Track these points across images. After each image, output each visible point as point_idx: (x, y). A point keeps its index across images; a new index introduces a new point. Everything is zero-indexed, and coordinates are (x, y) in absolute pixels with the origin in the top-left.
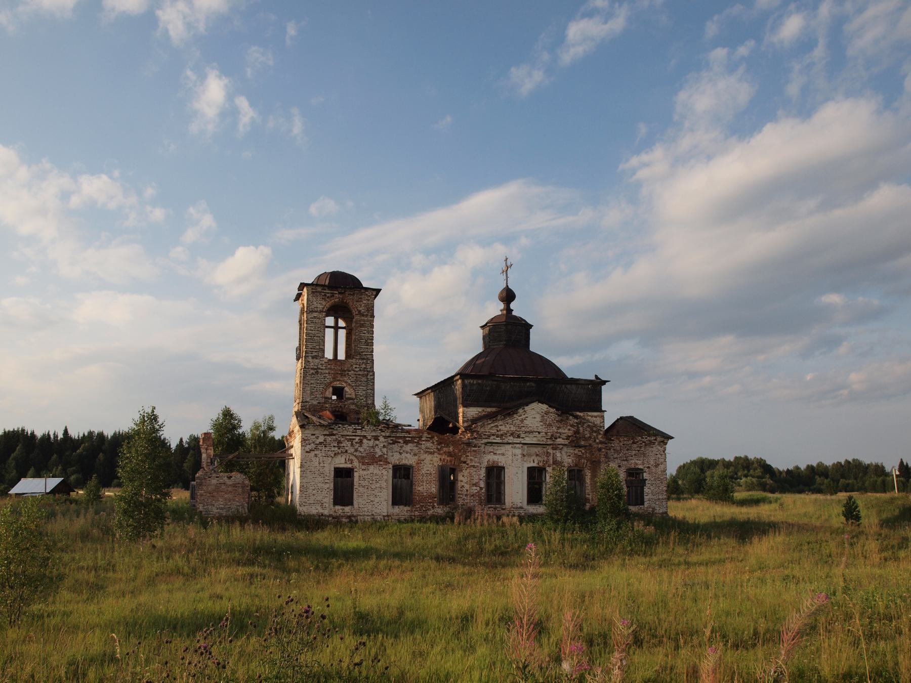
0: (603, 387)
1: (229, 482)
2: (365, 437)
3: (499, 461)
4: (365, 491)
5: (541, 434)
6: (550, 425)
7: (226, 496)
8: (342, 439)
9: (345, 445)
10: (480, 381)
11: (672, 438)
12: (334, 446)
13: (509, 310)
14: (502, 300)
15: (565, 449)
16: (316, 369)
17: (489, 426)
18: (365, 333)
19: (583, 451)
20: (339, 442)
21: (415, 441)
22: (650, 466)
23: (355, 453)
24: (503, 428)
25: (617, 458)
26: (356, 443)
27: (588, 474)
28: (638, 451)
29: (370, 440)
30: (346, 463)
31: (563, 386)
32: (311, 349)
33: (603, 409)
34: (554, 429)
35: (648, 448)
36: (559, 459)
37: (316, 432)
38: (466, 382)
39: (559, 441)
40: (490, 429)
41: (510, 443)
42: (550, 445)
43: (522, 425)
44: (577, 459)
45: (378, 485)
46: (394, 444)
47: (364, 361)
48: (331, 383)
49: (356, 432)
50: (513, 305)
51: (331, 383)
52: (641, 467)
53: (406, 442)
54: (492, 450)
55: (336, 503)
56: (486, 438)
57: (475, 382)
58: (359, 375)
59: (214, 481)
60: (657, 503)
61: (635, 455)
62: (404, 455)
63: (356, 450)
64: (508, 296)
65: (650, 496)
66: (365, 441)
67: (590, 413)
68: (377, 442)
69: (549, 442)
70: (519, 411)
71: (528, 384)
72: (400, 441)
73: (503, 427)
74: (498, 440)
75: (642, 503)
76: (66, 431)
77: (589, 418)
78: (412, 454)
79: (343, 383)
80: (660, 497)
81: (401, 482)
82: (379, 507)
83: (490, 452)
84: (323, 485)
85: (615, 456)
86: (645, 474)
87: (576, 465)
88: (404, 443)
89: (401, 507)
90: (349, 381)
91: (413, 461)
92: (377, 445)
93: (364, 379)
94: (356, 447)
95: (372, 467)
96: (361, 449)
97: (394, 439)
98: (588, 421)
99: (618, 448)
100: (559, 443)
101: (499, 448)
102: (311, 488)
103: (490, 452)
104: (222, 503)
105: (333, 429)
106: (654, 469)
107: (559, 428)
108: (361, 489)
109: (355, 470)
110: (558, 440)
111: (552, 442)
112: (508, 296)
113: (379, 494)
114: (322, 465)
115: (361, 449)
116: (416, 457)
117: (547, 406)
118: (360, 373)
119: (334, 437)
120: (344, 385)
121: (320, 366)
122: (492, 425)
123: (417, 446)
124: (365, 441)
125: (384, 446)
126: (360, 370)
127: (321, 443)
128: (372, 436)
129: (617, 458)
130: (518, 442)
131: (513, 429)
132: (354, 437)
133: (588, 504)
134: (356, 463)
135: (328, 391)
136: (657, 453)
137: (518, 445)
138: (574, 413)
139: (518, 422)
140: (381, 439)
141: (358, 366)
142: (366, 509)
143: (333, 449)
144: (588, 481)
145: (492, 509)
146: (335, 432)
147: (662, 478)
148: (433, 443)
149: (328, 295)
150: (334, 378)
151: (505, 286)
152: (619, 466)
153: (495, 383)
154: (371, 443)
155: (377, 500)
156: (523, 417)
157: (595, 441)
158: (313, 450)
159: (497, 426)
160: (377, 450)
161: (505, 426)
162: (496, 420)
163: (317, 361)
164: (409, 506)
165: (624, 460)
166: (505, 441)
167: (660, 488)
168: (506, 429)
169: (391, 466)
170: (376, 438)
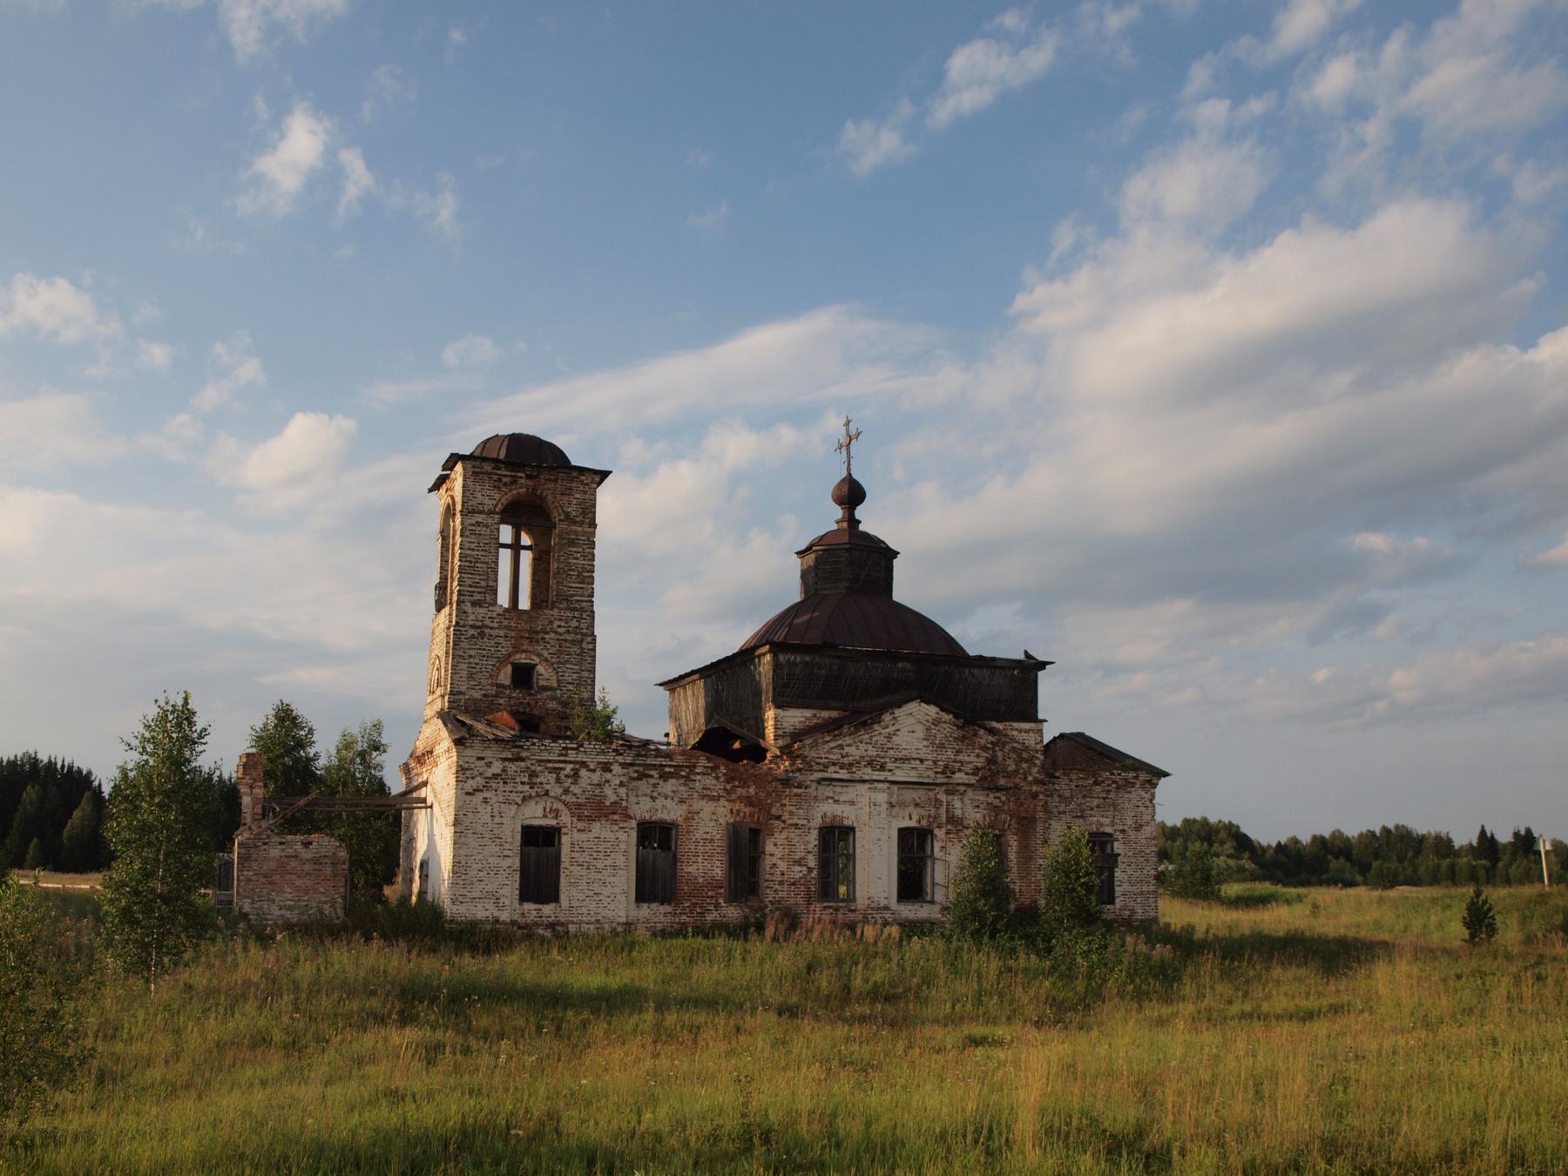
0: (1041, 674)
1: (306, 854)
2: (584, 764)
4: (584, 872)
5: (926, 763)
6: (942, 746)
9: (543, 780)
10: (808, 658)
11: (1166, 775)
12: (523, 783)
14: (839, 500)
20: (533, 774)
21: (683, 773)
22: (1125, 828)
23: (563, 797)
25: (1064, 812)
26: (567, 776)
29: (594, 771)
30: (545, 816)
33: (1041, 716)
36: (958, 813)
38: (782, 658)
39: (960, 777)
43: (889, 745)
48: (509, 655)
49: (566, 755)
50: (860, 512)
52: (1109, 830)
53: (665, 777)
54: (831, 794)
58: (566, 640)
63: (566, 791)
64: (851, 495)
65: (1126, 887)
66: (583, 772)
67: (1016, 725)
68: (608, 776)
69: (941, 779)
71: (900, 665)
73: (853, 748)
74: (843, 774)
77: (1015, 733)
79: (534, 657)
80: (1145, 888)
83: (828, 798)
85: (1061, 809)
88: (661, 777)
89: (654, 906)
90: (545, 654)
91: (678, 813)
92: (607, 781)
94: (566, 785)
95: (596, 826)
97: (641, 769)
98: (1013, 740)
100: (960, 781)
103: (828, 798)
104: (290, 896)
107: (959, 752)
110: (958, 775)
111: (945, 780)
112: (851, 495)
113: (611, 879)
118: (568, 637)
119: (523, 764)
121: (488, 622)
122: (832, 744)
123: (685, 785)
124: (583, 772)
126: (568, 632)
127: (495, 776)
128: (599, 763)
129: (1064, 812)
130: (882, 778)
131: (872, 752)
132: (561, 765)
134: (566, 818)
136: (1140, 804)
137: (880, 785)
138: (987, 723)
139: (881, 740)
140: (616, 769)
141: (563, 624)
142: (585, 910)
145: (831, 910)
146: (524, 754)
147: (1147, 851)
148: (717, 778)
149: (504, 480)
151: (844, 474)
153: (838, 661)
154: (596, 777)
155: (606, 891)
156: (891, 729)
158: (481, 791)
159: (841, 747)
160: (608, 791)
161: (857, 747)
164: (670, 904)
165: (1077, 817)
166: (857, 776)
169: (634, 824)
170: (606, 768)
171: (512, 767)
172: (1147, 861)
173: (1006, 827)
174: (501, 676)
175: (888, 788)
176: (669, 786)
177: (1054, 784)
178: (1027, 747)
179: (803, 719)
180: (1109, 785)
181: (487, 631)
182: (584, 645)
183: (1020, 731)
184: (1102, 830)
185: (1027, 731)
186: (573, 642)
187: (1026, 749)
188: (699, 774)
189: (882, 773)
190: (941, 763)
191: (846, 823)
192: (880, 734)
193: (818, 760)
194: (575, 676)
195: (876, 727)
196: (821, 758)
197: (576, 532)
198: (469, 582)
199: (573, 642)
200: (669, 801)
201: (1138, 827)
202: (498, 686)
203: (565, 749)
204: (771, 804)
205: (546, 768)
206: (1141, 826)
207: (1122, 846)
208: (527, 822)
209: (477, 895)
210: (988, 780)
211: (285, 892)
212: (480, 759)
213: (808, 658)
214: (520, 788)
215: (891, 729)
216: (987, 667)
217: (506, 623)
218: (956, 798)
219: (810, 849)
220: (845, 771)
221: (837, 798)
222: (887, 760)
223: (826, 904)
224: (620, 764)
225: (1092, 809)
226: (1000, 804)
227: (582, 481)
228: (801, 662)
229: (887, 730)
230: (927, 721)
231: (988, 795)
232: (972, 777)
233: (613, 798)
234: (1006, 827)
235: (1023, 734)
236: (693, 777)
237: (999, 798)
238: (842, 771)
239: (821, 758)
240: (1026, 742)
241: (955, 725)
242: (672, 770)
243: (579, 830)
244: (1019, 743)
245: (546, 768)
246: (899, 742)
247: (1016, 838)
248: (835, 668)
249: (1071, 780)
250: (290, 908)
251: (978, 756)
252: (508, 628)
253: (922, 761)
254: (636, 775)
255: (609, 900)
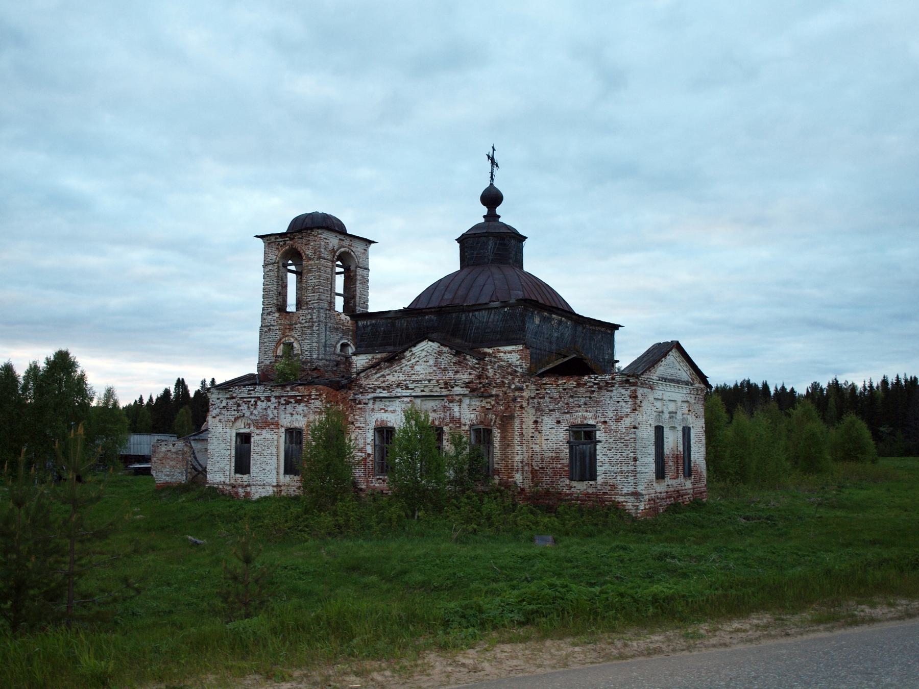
1: (173, 450)
2: (259, 398)
3: (388, 420)
4: (259, 457)
5: (432, 382)
6: (445, 370)
7: (171, 463)
8: (241, 402)
9: (243, 408)
10: (374, 322)
12: (234, 410)
13: (492, 217)
15: (466, 401)
16: (268, 326)
17: (375, 377)
18: (311, 280)
19: (493, 403)
20: (239, 405)
21: (305, 400)
22: (607, 420)
23: (251, 417)
24: (390, 378)
25: (553, 410)
26: (252, 405)
27: (497, 433)
28: (590, 398)
29: (263, 401)
30: (245, 427)
31: (471, 314)
32: (267, 305)
34: (451, 374)
35: (604, 392)
36: (457, 415)
37: (220, 396)
38: (360, 323)
39: (458, 390)
40: (376, 380)
41: (399, 397)
42: (446, 396)
43: (413, 372)
44: (483, 414)
45: (269, 452)
46: (288, 404)
47: (310, 311)
48: (280, 340)
49: (250, 394)
50: (499, 210)
51: (280, 340)
52: (591, 422)
53: (298, 402)
54: (383, 407)
55: (236, 472)
56: (373, 392)
57: (369, 324)
58: (305, 327)
59: (163, 449)
60: (619, 478)
61: (585, 404)
62: (295, 416)
63: (252, 414)
64: (492, 198)
65: (607, 467)
66: (259, 403)
67: (501, 349)
68: (269, 404)
69: (445, 392)
70: (405, 354)
71: (427, 317)
72: (292, 400)
73: (391, 376)
74: (385, 394)
75: (593, 477)
76: (792, 389)
77: (502, 354)
78: (302, 415)
79: (291, 339)
80: (625, 468)
81: (292, 447)
82: (269, 476)
83: (381, 409)
84: (225, 451)
85: (552, 407)
86: (598, 433)
87: (482, 422)
88: (296, 402)
89: (292, 476)
90: (296, 336)
91: (303, 423)
92: (269, 407)
93: (309, 331)
94: (252, 410)
95: (264, 432)
96: (255, 412)
97: (287, 398)
98: (501, 360)
99: (556, 395)
100: (458, 393)
101: (391, 403)
102: (216, 455)
103: (381, 409)
104: (168, 470)
105: (231, 391)
106: (613, 425)
107: (457, 372)
108: (255, 455)
109: (252, 435)
110: (456, 389)
111: (448, 393)
112: (492, 198)
113: (269, 461)
114: (225, 430)
115: (255, 412)
116: (306, 419)
117: (439, 345)
118: (306, 325)
119: (234, 400)
120: (292, 340)
121: (272, 323)
122: (378, 375)
123: (306, 406)
124: (259, 403)
125: (275, 408)
126: (306, 322)
127: (224, 407)
128: (266, 397)
129: (553, 410)
130: (408, 394)
131: (402, 378)
132: (249, 400)
133: (496, 477)
135: (279, 348)
136: (620, 400)
137: (406, 399)
138: (481, 349)
139: (407, 369)
140: (273, 400)
141: (304, 318)
142: (258, 478)
143: (233, 413)
144: (497, 443)
145: (381, 481)
146: (234, 395)
147: (627, 438)
148: (321, 401)
149: (281, 243)
150: (283, 334)
151: (488, 185)
152: (558, 422)
153: (389, 321)
154: (264, 405)
155: (268, 468)
156: (413, 361)
157: (509, 387)
158: (218, 415)
159: (383, 376)
160: (269, 412)
161: (393, 376)
162: (381, 368)
163: (270, 317)
164: (298, 475)
165: (565, 413)
166: (393, 394)
167: (624, 455)
168: (394, 379)
169: (283, 430)
170: (268, 399)
171: (231, 402)
172: (627, 446)
173: (492, 423)
174: (278, 351)
175: (411, 401)
176: (301, 408)
177: (545, 389)
178: (510, 364)
179: (367, 361)
180: (592, 387)
181: (271, 327)
182: (314, 328)
183: (505, 353)
184: (585, 422)
185: (510, 352)
186: (308, 327)
187: (510, 365)
188: (313, 399)
189: (408, 391)
190: (441, 381)
191: (389, 425)
192: (406, 365)
193: (368, 386)
194: (309, 346)
195: (403, 361)
196: (369, 384)
197: (311, 265)
198: (266, 302)
199: (308, 327)
200: (299, 416)
201: (619, 419)
202: (276, 356)
203: (249, 390)
204: (348, 415)
205: (244, 402)
206: (621, 418)
207: (603, 435)
208: (238, 431)
209: (216, 469)
210: (476, 390)
211: (166, 468)
212: (218, 399)
213: (374, 322)
214: (233, 413)
215: (413, 361)
216: (485, 309)
217: (280, 322)
218: (455, 404)
219: (369, 442)
220: (386, 392)
221: (386, 409)
222: (408, 382)
223: (378, 477)
224: (275, 397)
225: (580, 406)
226: (490, 407)
227: (313, 235)
228: (370, 325)
229: (410, 362)
230: (435, 353)
231: (482, 401)
232: (465, 389)
233: (271, 416)
234: (492, 423)
235: (507, 354)
236: (310, 401)
237: (490, 402)
238: (384, 392)
239: (369, 384)
240: (510, 360)
241: (452, 354)
242: (300, 398)
243: (257, 434)
244: (505, 361)
245: (244, 402)
246: (419, 369)
247: (499, 431)
248: (389, 325)
249: (558, 386)
250: (168, 476)
251: (470, 374)
252: (281, 324)
253: (429, 381)
254: (284, 402)
255: (269, 473)
